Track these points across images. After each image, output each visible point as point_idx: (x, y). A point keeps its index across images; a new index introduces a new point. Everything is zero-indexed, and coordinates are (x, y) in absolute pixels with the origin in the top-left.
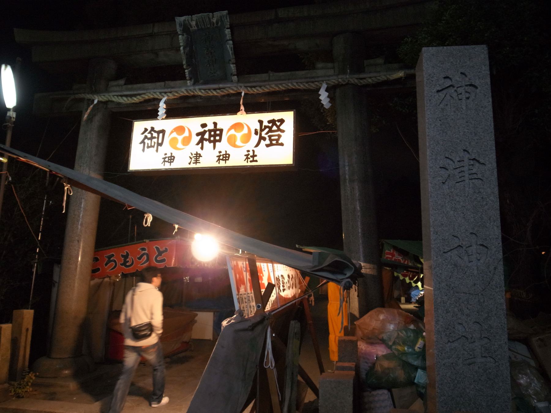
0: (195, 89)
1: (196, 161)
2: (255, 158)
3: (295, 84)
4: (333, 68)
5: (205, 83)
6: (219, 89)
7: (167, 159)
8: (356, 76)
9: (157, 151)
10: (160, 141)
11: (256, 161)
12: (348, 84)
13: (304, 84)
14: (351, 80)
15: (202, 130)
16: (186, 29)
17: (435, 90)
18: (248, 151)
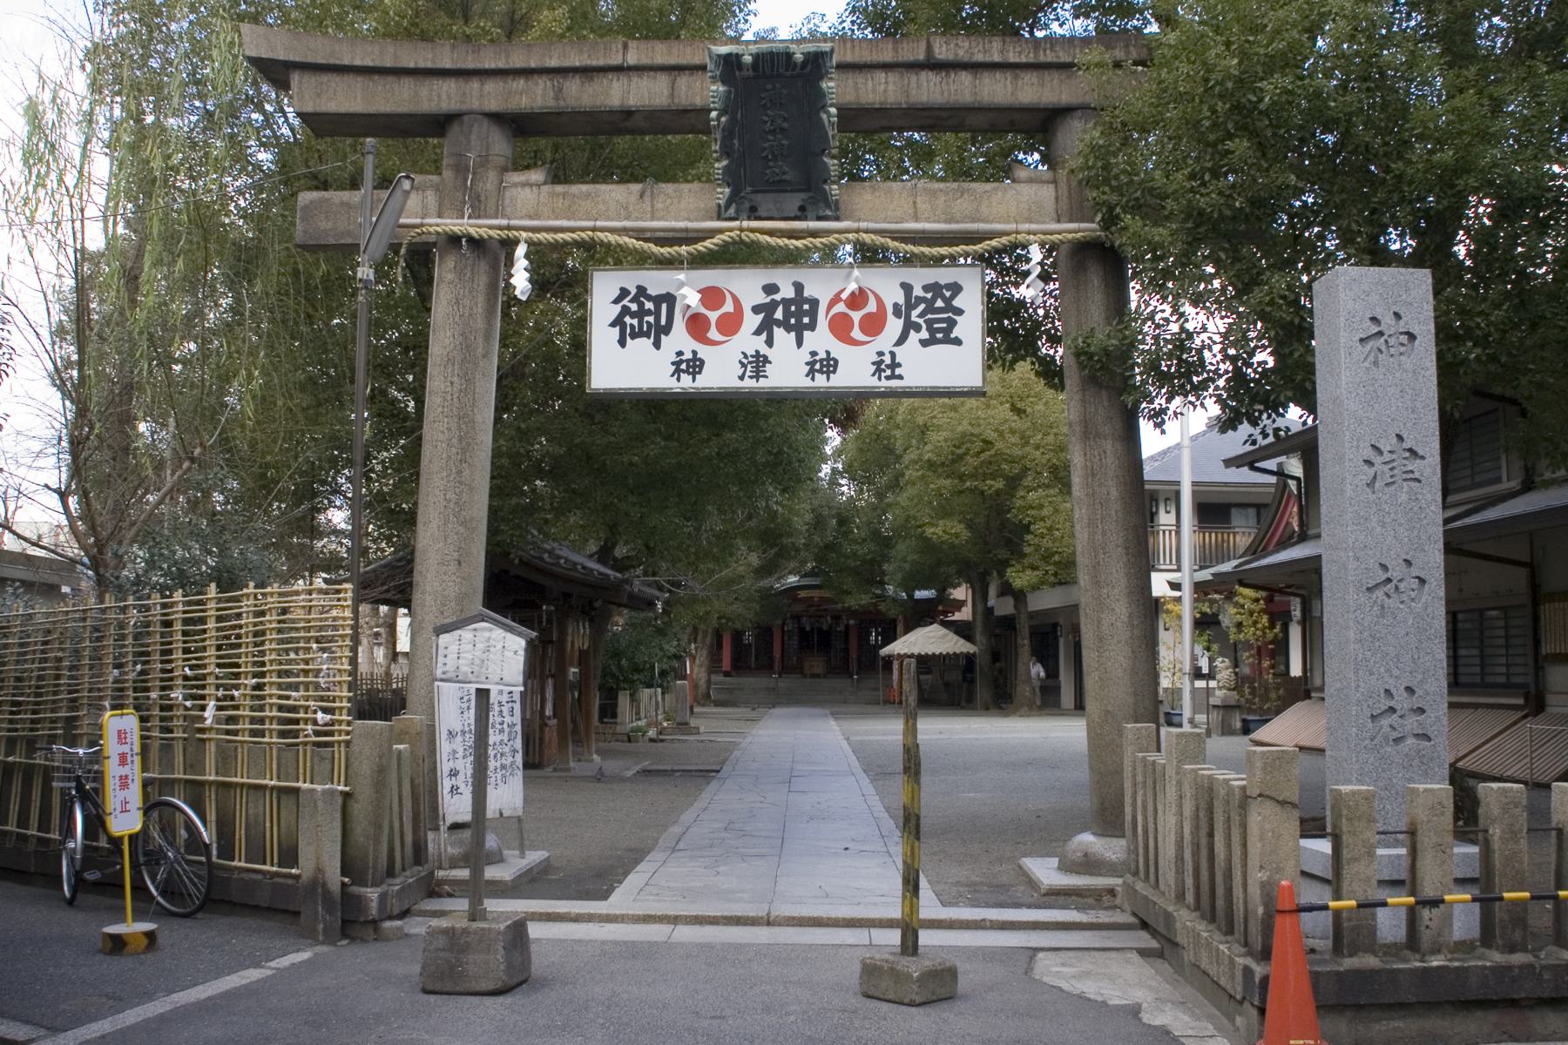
2: (898, 371)
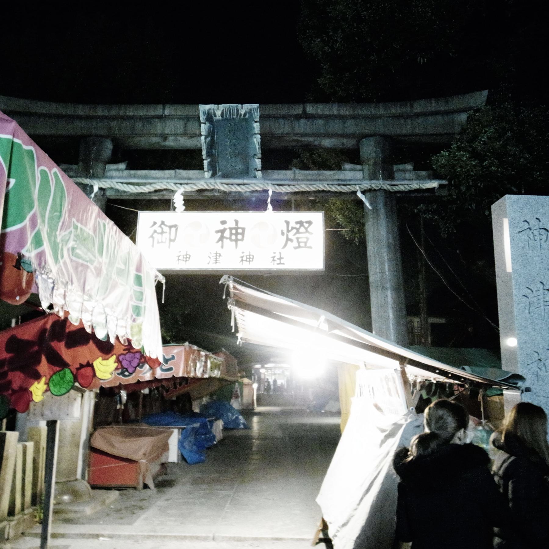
0: (216, 183)
1: (216, 260)
2: (282, 261)
3: (326, 186)
4: (362, 170)
5: (225, 176)
6: (244, 184)
7: (181, 258)
8: (389, 182)
9: (169, 247)
10: (173, 238)
11: (283, 264)
12: (380, 189)
13: (336, 186)
14: (384, 186)
15: (222, 227)
16: (210, 118)
17: (517, 232)
18: (274, 253)
